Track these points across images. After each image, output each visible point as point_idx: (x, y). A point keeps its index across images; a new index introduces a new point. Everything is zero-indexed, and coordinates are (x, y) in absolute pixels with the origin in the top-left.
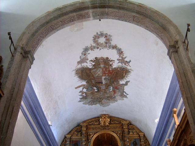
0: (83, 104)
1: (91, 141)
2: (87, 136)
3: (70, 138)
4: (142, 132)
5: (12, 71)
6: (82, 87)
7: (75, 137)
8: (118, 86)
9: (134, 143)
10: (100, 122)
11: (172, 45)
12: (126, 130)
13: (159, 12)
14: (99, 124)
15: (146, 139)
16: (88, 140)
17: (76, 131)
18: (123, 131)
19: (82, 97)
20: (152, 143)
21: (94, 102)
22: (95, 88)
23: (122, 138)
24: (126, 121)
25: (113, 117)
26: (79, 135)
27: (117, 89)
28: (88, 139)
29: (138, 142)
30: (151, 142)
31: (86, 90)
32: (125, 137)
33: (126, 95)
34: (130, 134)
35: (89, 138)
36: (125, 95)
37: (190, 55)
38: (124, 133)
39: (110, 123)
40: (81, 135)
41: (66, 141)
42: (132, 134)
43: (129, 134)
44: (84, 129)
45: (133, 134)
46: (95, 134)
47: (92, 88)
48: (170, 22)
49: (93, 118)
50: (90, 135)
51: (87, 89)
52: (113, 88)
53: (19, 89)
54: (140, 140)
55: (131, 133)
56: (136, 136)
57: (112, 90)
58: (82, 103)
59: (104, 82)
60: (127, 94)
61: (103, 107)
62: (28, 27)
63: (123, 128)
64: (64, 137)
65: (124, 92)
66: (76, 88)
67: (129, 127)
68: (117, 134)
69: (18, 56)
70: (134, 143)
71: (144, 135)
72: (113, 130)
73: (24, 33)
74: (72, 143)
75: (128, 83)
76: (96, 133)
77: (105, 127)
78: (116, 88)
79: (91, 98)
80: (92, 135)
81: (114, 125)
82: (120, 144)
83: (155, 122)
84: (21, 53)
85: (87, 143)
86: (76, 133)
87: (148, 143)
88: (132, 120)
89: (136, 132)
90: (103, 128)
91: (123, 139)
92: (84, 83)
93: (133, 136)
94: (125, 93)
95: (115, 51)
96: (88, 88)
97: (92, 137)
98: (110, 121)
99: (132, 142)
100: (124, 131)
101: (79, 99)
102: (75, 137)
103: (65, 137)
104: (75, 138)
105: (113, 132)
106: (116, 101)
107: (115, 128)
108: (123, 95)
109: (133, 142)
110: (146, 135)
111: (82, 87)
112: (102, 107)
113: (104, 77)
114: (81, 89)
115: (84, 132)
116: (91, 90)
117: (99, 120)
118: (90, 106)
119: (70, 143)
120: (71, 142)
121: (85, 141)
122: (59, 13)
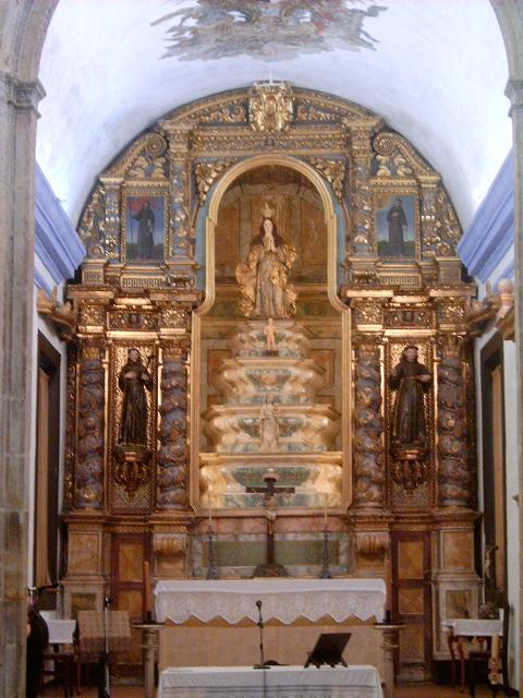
0: (180, 60)
1: (209, 199)
2: (194, 176)
3: (122, 187)
4: (433, 170)
6: (182, 16)
7: (140, 183)
8: (336, 12)
9: (395, 214)
10: (247, 116)
11: (517, 81)
12: (363, 160)
14: (246, 123)
15: (448, 200)
16: (197, 197)
17: (143, 153)
18: (349, 163)
19: (176, 43)
20: (473, 228)
21: (226, 50)
22: (235, 14)
23: (343, 191)
24: (369, 113)
25: (309, 91)
26: (158, 172)
27: (332, 19)
31: (196, 20)
32: (354, 190)
33: (371, 41)
34: (380, 173)
35: (200, 188)
36: (364, 41)
38: (355, 173)
39: (294, 122)
40: (167, 174)
41: (102, 199)
42: (389, 173)
43: (373, 173)
44: (178, 148)
45: (394, 175)
47: (223, 13)
49: (222, 94)
50: (205, 173)
51: (202, 18)
52: (315, 14)
53: (26, 239)
54: (421, 203)
55: (383, 170)
56: (405, 185)
57: (309, 20)
58: (176, 57)
60: (374, 40)
61: (268, 61)
64: (91, 183)
65: (359, 30)
66: (152, 24)
67: (375, 144)
68: (321, 172)
70: (395, 214)
71: (440, 184)
72: (305, 152)
75: (381, 13)
76: (232, 164)
77: (269, 141)
78: (329, 17)
79: (217, 40)
80: (214, 175)
81: (314, 133)
82: (332, 217)
83: (421, 365)
84: (9, 103)
85: (191, 212)
86: (142, 161)
87: (452, 218)
88: (391, 117)
89: (407, 165)
90: (262, 144)
91: (345, 194)
93: (391, 179)
94: (367, 35)
96: (205, 15)
97: (216, 180)
98: (295, 109)
99: (386, 208)
100: (355, 164)
101: (165, 51)
102: (140, 183)
103: (98, 183)
104: (139, 184)
105: (308, 162)
106: (326, 49)
107: (316, 143)
109: (391, 212)
110: (445, 182)
111: (182, 16)
112: (262, 62)
114: (176, 21)
115: (179, 163)
116: (218, 20)
117: (246, 106)
118: (211, 62)
119: (120, 210)
120: (124, 204)
121: (186, 202)
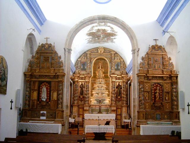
5: (66, 62)
12: (113, 57)
13: (131, 29)
16: (91, 62)
17: (84, 56)
18: (111, 58)
28: (91, 62)
29: (119, 64)
30: (127, 66)
37: (138, 58)
41: (78, 62)
43: (115, 59)
44: (88, 55)
45: (117, 59)
46: (95, 58)
48: (135, 36)
50: (92, 59)
59: (102, 36)
62: (68, 36)
63: (111, 55)
69: (67, 53)
71: (123, 61)
72: (105, 56)
73: (67, 40)
74: (82, 63)
89: (119, 58)
91: (111, 62)
92: (91, 37)
93: (117, 60)
95: (109, 27)
99: (116, 64)
103: (77, 60)
104: (83, 60)
108: (112, 41)
113: (102, 35)
114: (89, 39)
115: (88, 57)
117: (97, 50)
121: (89, 63)
122: (82, 23)
